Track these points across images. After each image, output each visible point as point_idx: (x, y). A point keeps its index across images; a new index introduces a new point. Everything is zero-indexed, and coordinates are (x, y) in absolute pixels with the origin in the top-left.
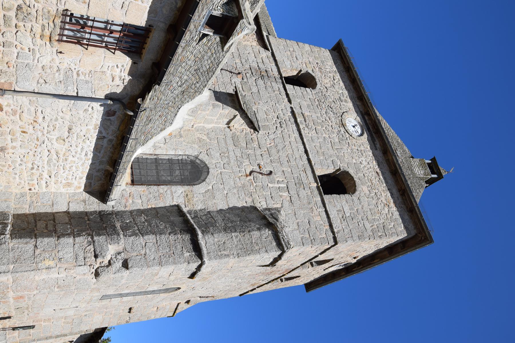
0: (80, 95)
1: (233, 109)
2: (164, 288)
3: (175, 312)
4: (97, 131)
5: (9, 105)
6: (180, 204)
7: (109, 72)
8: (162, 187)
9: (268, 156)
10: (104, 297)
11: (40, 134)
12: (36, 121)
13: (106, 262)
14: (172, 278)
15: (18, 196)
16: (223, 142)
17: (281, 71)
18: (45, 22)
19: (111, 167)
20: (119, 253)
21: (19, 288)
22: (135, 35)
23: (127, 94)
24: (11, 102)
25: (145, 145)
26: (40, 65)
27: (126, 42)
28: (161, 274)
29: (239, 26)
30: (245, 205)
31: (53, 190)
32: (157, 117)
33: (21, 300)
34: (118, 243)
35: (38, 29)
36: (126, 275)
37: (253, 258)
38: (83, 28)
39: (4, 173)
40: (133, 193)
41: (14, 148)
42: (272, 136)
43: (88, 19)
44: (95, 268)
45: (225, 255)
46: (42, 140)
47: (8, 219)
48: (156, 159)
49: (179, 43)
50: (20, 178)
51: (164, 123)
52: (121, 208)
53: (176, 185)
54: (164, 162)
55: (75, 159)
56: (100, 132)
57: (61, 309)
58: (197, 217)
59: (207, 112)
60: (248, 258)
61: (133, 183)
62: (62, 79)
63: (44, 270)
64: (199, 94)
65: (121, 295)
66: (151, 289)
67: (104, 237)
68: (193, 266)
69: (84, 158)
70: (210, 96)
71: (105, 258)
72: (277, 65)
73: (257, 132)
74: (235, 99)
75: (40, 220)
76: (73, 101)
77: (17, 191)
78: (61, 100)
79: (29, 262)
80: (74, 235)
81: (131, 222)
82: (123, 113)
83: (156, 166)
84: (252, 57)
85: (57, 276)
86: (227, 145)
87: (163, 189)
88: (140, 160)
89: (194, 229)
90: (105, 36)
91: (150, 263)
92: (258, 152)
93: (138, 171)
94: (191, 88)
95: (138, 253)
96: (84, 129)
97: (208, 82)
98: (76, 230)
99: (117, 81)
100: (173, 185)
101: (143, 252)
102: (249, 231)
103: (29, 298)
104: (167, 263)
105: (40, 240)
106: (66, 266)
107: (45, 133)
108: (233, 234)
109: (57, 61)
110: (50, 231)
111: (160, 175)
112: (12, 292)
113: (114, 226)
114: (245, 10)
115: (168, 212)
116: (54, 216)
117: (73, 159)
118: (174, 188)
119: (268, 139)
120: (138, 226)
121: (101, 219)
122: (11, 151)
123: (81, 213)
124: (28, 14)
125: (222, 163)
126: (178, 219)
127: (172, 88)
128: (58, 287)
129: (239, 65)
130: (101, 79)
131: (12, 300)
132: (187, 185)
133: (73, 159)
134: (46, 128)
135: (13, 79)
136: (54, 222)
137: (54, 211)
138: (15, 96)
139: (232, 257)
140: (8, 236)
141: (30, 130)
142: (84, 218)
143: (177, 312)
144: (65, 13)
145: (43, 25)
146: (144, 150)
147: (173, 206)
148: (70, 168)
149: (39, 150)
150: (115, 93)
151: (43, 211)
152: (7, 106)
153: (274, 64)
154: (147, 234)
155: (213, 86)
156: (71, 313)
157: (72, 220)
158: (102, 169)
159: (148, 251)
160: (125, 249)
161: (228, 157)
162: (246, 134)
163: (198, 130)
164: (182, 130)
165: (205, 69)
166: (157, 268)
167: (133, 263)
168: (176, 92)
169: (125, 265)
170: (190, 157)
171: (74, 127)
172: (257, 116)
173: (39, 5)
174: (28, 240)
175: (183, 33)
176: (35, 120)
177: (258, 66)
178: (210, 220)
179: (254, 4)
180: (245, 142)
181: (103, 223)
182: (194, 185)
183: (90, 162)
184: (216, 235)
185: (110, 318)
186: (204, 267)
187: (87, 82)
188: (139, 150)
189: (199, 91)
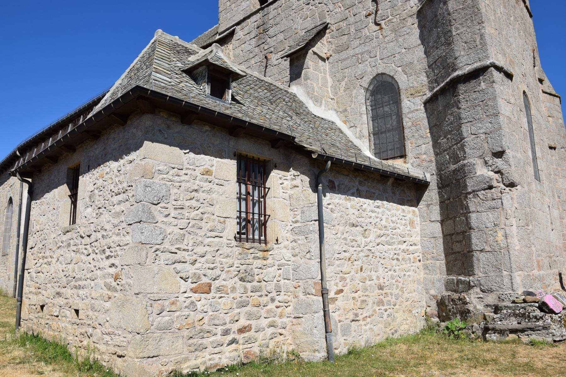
0: (317, 218)
1: (307, 57)
2: (524, 110)
3: (554, 96)
4: (352, 197)
5: (336, 284)
6: (423, 101)
7: (289, 192)
8: (404, 124)
9: (355, 7)
10: (537, 177)
11: (362, 254)
12: (349, 259)
13: (497, 176)
14: (512, 101)
15: (428, 272)
16: (345, 62)
17: (254, 10)
18: (250, 256)
19: (388, 180)
20: (486, 163)
21: (529, 264)
22: (246, 169)
23: (309, 171)
24: (333, 282)
25: (360, 147)
26: (293, 259)
27: (256, 178)
28: (508, 114)
29: (216, 63)
30: (416, 25)
31: (419, 238)
32: (328, 138)
33: (541, 263)
34: (474, 164)
35: (259, 263)
36: (511, 153)
37: (483, 4)
38: (249, 222)
39: (404, 286)
40: (415, 155)
41: (378, 278)
42: (331, 7)
43: (239, 217)
44: (504, 187)
45: (481, 39)
46: (367, 251)
47: (453, 279)
48: (374, 135)
49: (247, 122)
50: (409, 271)
51: (333, 131)
52: (433, 166)
53: (401, 108)
54: (376, 125)
55: (384, 218)
56: (353, 195)
57: (552, 223)
58: (436, 80)
59: (315, 85)
60: (483, 10)
61: (403, 156)
62: (303, 237)
63: (509, 241)
64: (296, 97)
65: (535, 159)
66: (526, 125)
67: (468, 180)
68: (497, 75)
69: (382, 209)
70: (296, 84)
71: (492, 178)
72: (248, 17)
73: (329, 25)
74: (295, 56)
75: (452, 249)
76: (324, 224)
77: (422, 273)
78: (325, 236)
79: (499, 257)
80: (467, 212)
81: (448, 154)
82: (329, 173)
83: (381, 133)
84: (246, 47)
85: (514, 227)
86: (348, 58)
87: (407, 123)
88: (377, 152)
89: (451, 80)
90: (253, 200)
91: (496, 126)
92: (352, 19)
93: (389, 152)
94: (291, 106)
95: (485, 141)
96: (351, 211)
97: (281, 89)
98: (462, 211)
99: (297, 182)
100: (401, 112)
101: (483, 136)
102: (449, 14)
103: (539, 255)
104: (495, 107)
105: (474, 247)
106: (503, 218)
107: (360, 249)
108: (454, 33)
109: (286, 243)
110: (464, 238)
111: (391, 128)
112: (533, 272)
113: (454, 171)
114: (198, 60)
115: (433, 113)
116: (447, 235)
117: (384, 219)
118: (405, 111)
119: (335, 11)
120: (453, 145)
121: (448, 186)
122: (381, 280)
123: (441, 208)
124: (246, 272)
125: (370, 60)
126: (441, 101)
127: (295, 126)
128: (528, 225)
129: (257, 59)
130: (298, 199)
131: (542, 272)
132: (400, 96)
133: (384, 219)
134: (355, 249)
135: (310, 282)
136: (453, 234)
137: (441, 235)
138: (327, 279)
139: (483, 31)
140: (471, 278)
141: (359, 263)
142: (447, 205)
143: (554, 92)
144: (238, 239)
145: (254, 258)
146: (365, 148)
147: (426, 109)
148: (393, 222)
149: (378, 254)
150: (310, 183)
151: (442, 246)
152: (337, 286)
153: (249, 20)
154: (461, 134)
155: (285, 83)
156: (556, 213)
157: (450, 217)
158: (392, 189)
159: (482, 131)
160: (480, 157)
161: (362, 54)
162: (333, 38)
163: (336, 93)
164: (338, 110)
165: (269, 94)
166: (501, 118)
167: (497, 146)
168: (298, 121)
169: (499, 154)
170: (367, 98)
171: (351, 221)
172: (310, 29)
173: (236, 262)
174: (474, 259)
175: (236, 119)
176: (347, 259)
177: (254, 38)
178: (439, 64)
179: (189, 52)
180: (342, 37)
181: (452, 183)
182: (399, 88)
183: (385, 202)
184: (457, 54)
185: (562, 170)
186: (497, 63)
187: (303, 212)
188: (367, 152)
189: (293, 97)
